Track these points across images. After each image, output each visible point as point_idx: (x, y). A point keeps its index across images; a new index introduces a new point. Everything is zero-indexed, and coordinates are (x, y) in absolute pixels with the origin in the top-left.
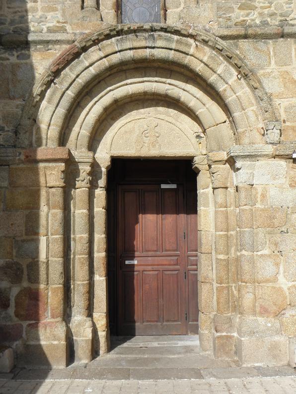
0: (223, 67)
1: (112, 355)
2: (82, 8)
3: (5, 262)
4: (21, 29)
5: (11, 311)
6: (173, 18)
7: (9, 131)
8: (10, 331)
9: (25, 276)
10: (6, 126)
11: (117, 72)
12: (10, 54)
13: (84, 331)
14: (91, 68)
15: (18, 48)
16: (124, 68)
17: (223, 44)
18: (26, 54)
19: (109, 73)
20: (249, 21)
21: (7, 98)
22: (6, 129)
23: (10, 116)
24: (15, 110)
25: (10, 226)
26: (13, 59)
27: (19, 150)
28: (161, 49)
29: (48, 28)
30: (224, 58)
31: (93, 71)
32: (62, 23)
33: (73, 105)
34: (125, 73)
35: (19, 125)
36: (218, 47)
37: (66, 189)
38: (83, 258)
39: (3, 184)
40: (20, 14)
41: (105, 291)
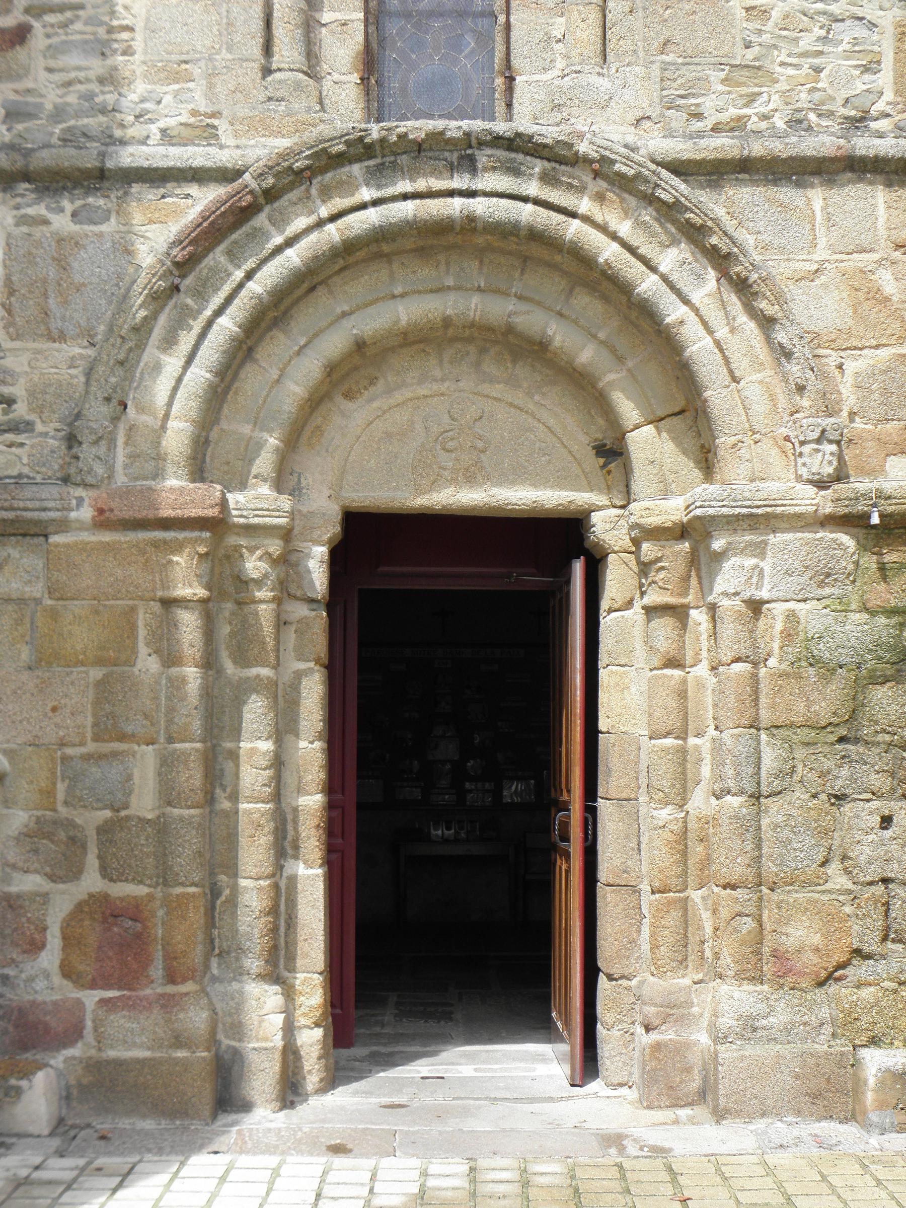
0: (673, 258)
1: (343, 1097)
2: (267, 71)
3: (33, 819)
4: (85, 135)
5: (50, 958)
6: (533, 100)
7: (46, 434)
8: (48, 1018)
9: (92, 860)
10: (38, 421)
11: (363, 261)
12: (53, 206)
13: (260, 1022)
14: (289, 252)
15: (74, 188)
16: (386, 248)
17: (674, 187)
18: (99, 207)
19: (341, 262)
20: (755, 119)
21: (42, 335)
22: (39, 427)
23: (51, 390)
24: (65, 373)
25: (50, 714)
26: (62, 223)
27: (80, 492)
28: (494, 197)
29: (163, 131)
30: (678, 229)
31: (294, 257)
32: (206, 115)
33: (235, 357)
34: (390, 262)
35: (78, 416)
36: (663, 196)
37: (211, 605)
38: (259, 810)
39: (27, 589)
40: (81, 88)
41: (322, 908)
